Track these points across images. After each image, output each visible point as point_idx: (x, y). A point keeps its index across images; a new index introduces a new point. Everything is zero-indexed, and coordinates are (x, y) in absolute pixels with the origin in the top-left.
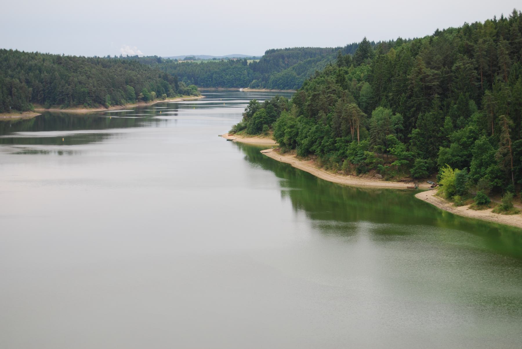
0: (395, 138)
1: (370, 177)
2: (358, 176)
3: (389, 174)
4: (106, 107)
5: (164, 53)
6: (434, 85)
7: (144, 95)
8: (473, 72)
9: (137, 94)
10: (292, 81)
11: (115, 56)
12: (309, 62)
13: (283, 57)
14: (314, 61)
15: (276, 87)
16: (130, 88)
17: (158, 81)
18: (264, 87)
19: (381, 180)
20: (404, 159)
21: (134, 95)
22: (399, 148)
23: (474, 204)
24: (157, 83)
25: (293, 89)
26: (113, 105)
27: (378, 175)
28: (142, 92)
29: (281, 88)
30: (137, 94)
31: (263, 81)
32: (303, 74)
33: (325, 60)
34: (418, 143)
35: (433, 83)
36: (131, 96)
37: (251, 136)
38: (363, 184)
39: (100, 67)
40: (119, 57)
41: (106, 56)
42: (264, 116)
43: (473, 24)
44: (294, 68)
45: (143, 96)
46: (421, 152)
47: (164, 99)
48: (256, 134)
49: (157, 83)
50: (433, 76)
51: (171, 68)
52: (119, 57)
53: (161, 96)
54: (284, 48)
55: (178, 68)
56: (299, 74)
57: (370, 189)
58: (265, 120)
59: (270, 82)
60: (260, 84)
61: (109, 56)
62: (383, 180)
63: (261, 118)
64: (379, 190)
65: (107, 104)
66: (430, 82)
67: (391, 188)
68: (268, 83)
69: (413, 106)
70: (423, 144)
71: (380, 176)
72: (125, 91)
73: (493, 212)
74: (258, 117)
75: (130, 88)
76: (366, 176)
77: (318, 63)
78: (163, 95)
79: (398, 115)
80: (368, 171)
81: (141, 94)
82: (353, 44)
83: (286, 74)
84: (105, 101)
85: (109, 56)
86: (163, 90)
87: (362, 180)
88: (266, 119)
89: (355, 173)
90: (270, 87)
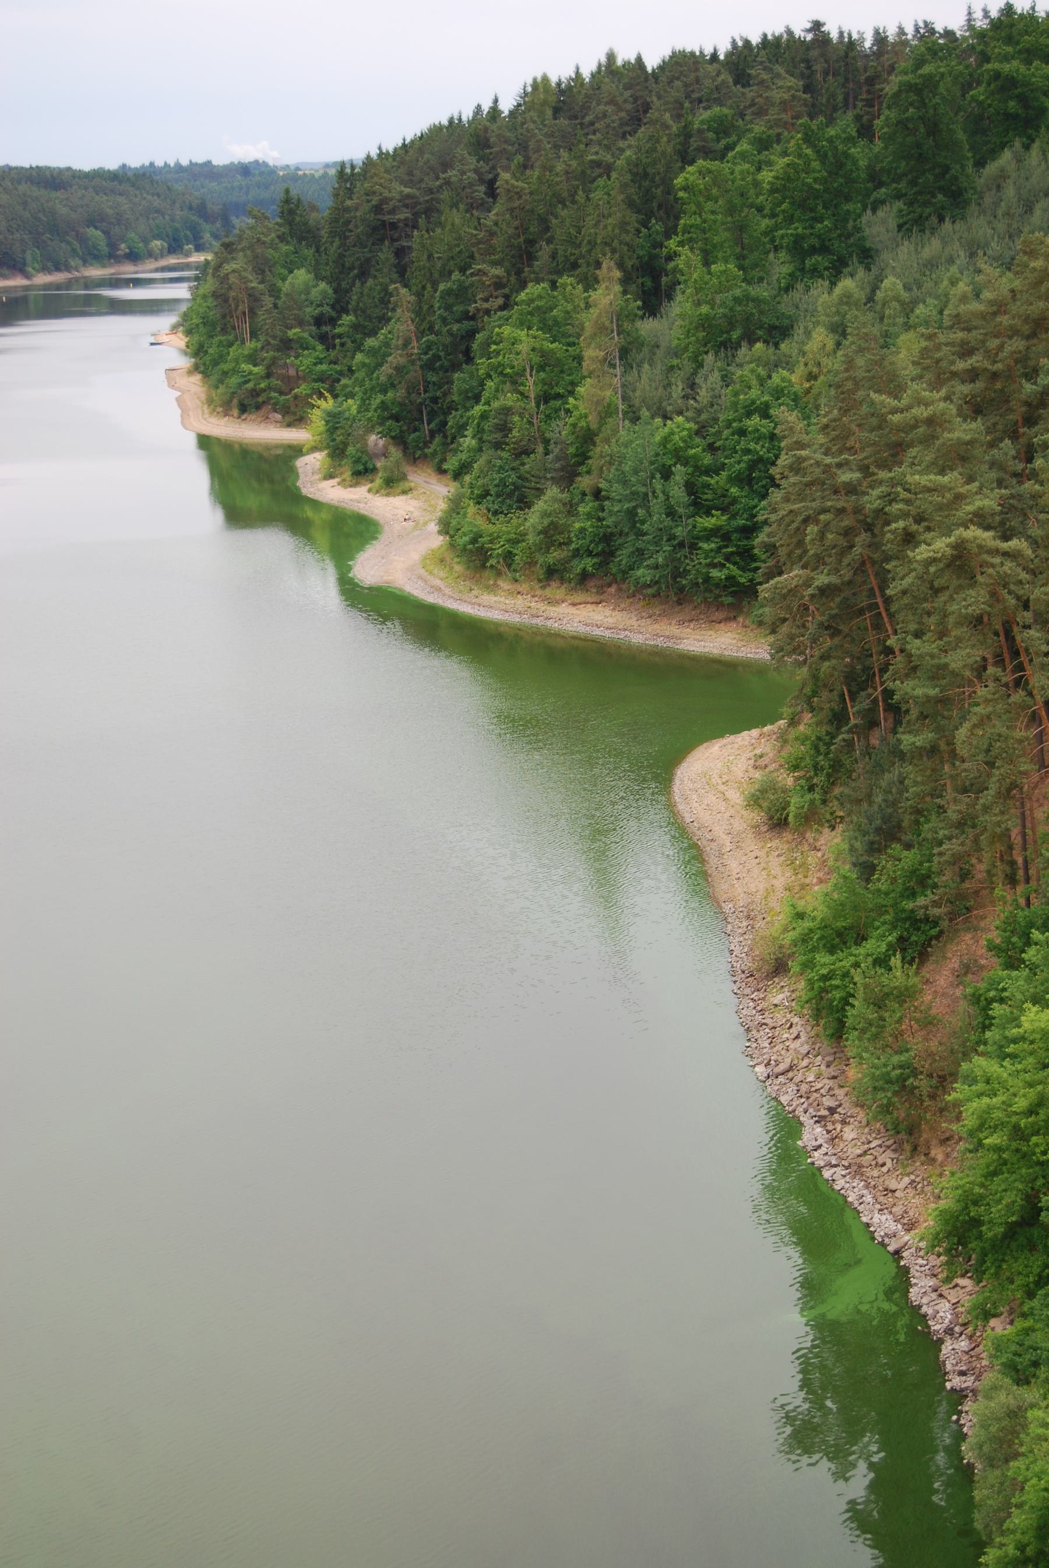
0: (306, 335)
1: (259, 419)
2: (239, 417)
3: (295, 413)
4: (28, 277)
5: (13, 163)
6: (399, 220)
7: (129, 248)
8: (476, 191)
9: (113, 246)
16: (95, 234)
17: (178, 217)
21: (104, 248)
23: (347, 475)
24: (172, 220)
26: (45, 269)
28: (125, 242)
30: (113, 246)
35: (397, 217)
36: (98, 250)
40: (172, 165)
41: (147, 164)
45: (127, 251)
47: (188, 255)
49: (172, 220)
50: (400, 201)
51: (259, 187)
52: (172, 165)
53: (182, 249)
55: (272, 188)
57: (260, 445)
61: (152, 164)
62: (281, 427)
64: (277, 446)
65: (30, 269)
66: (390, 212)
67: (295, 443)
71: (279, 417)
72: (82, 240)
73: (369, 491)
75: (95, 234)
78: (186, 247)
79: (323, 285)
80: (258, 407)
81: (123, 246)
84: (25, 264)
85: (152, 164)
86: (186, 236)
87: (243, 425)
89: (235, 412)
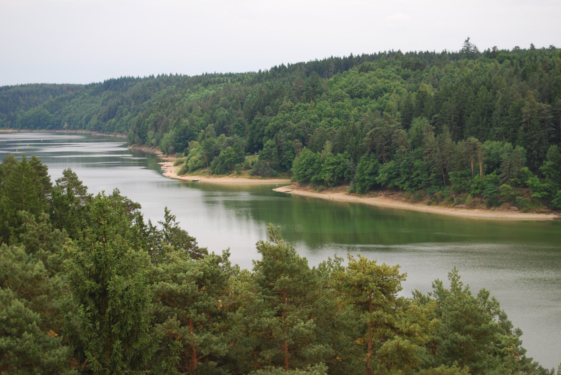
10: (45, 120)
11: (532, 45)
12: (62, 100)
13: (20, 93)
14: (66, 98)
15: (26, 127)
18: (11, 127)
19: (518, 212)
20: (543, 191)
22: (533, 180)
25: (46, 128)
27: (513, 207)
29: (31, 128)
31: (8, 120)
32: (57, 112)
33: (80, 97)
34: (552, 175)
37: (219, 176)
38: (504, 217)
39: (353, 72)
42: (234, 155)
43: (407, 53)
44: (44, 106)
46: (556, 184)
48: (225, 173)
54: (220, 73)
56: (52, 113)
58: (235, 159)
59: (17, 121)
60: (5, 124)
63: (230, 157)
67: (531, 220)
68: (16, 122)
69: (535, 139)
70: (557, 175)
74: (227, 156)
76: (501, 208)
77: (73, 100)
82: (111, 79)
83: (36, 113)
88: (236, 157)
90: (18, 127)
